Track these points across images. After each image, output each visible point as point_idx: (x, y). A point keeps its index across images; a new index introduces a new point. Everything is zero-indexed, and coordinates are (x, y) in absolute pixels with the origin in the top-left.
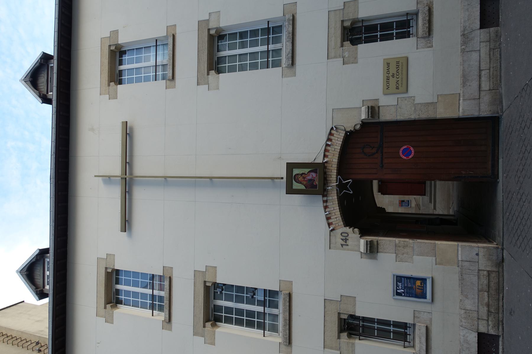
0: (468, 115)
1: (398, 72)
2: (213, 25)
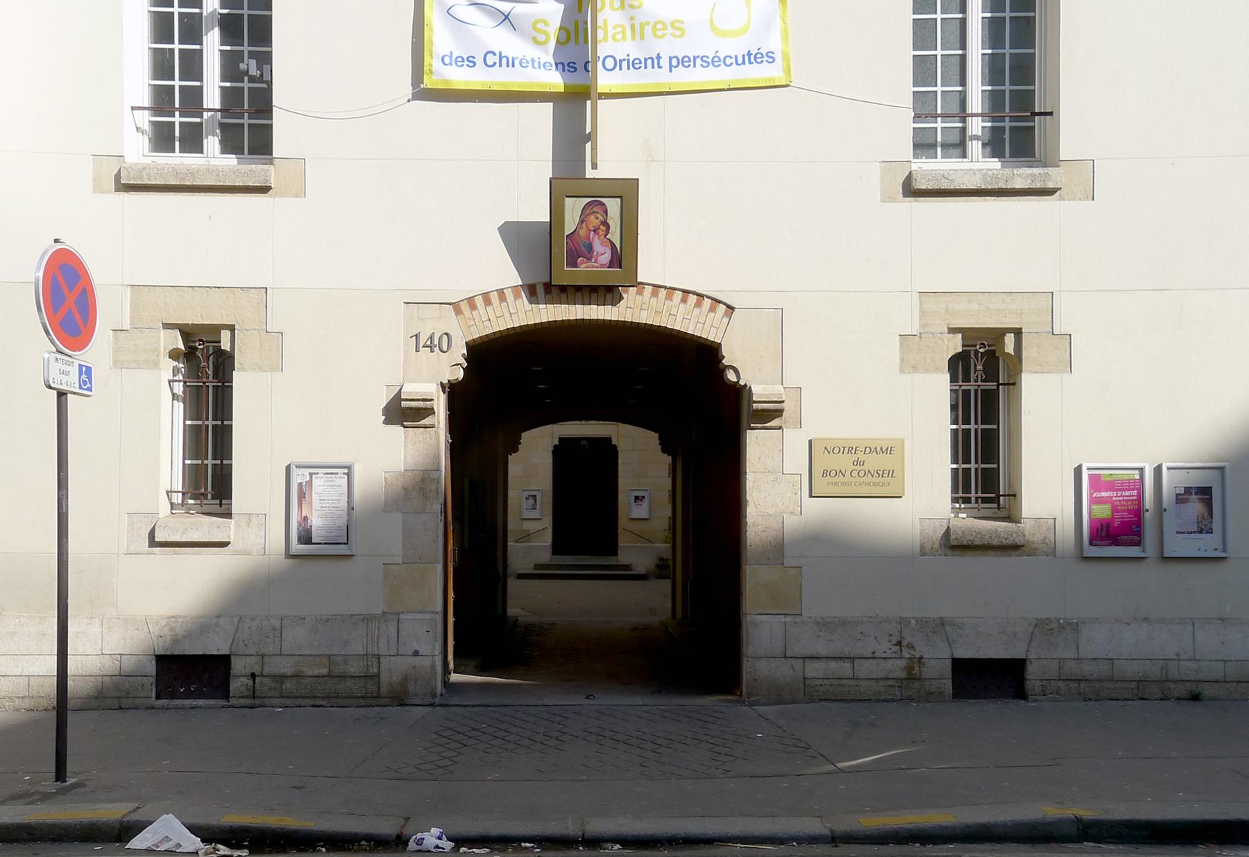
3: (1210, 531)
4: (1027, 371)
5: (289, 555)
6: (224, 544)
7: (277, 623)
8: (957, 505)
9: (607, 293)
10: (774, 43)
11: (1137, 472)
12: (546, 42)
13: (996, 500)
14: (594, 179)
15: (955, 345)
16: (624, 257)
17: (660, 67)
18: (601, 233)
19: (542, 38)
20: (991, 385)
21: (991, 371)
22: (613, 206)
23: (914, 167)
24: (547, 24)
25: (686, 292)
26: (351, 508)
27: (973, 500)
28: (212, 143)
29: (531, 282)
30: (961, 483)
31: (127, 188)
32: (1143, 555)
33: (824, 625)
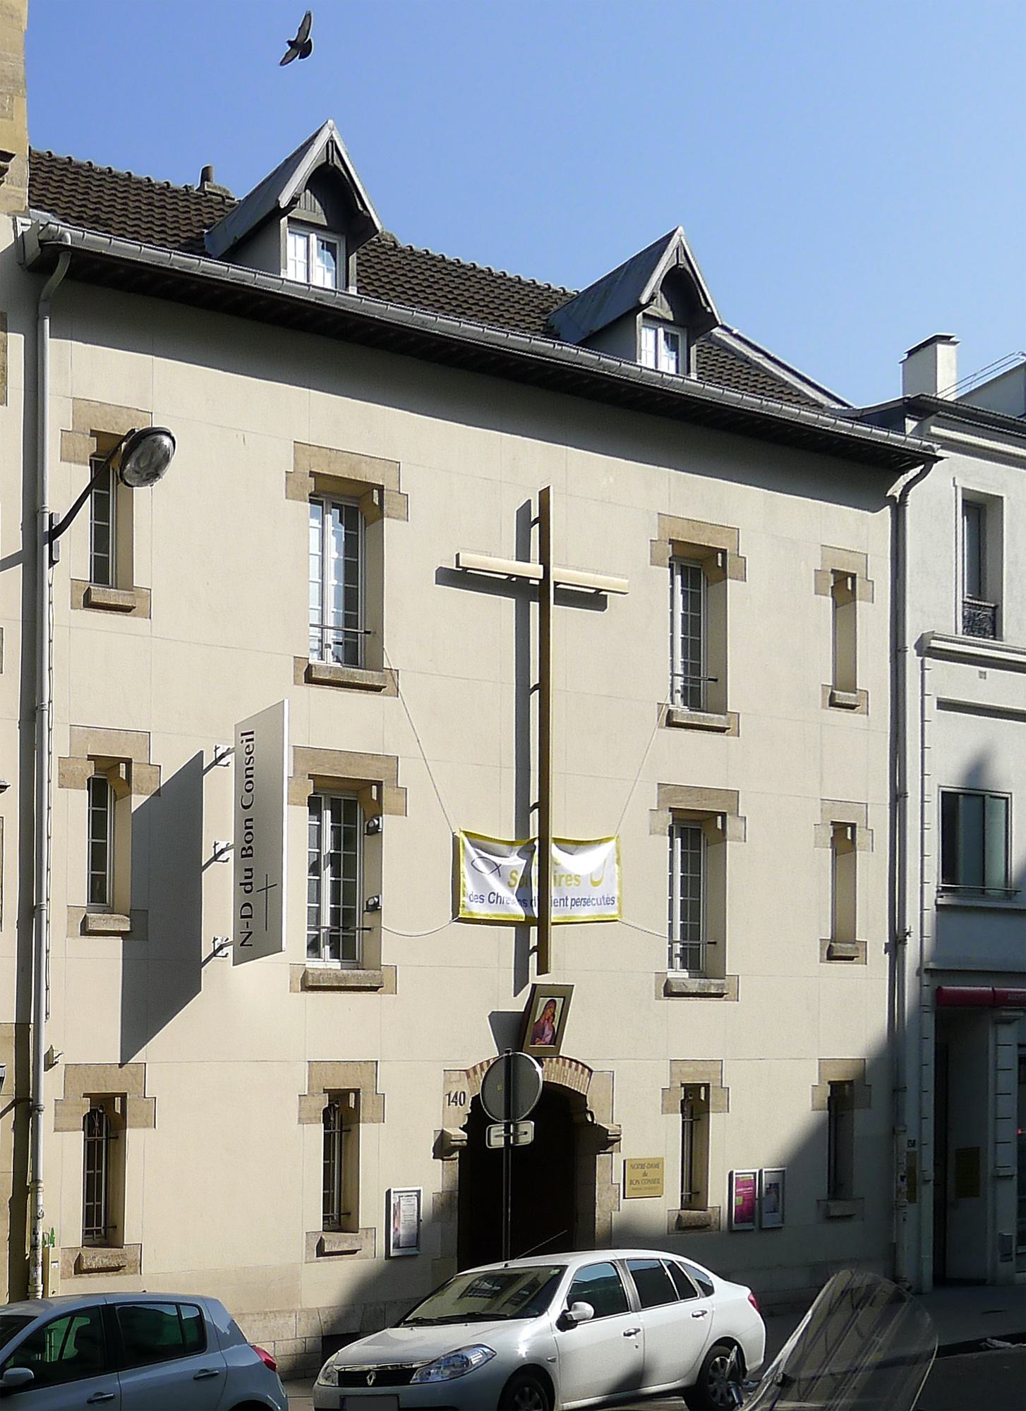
4: (131, 1127)
5: (388, 1256)
6: (354, 1252)
7: (382, 1307)
10: (616, 893)
11: (752, 1175)
12: (514, 886)
14: (553, 985)
16: (556, 1039)
19: (513, 882)
22: (559, 1001)
23: (669, 976)
25: (571, 1060)
26: (419, 1220)
28: (326, 950)
31: (307, 988)
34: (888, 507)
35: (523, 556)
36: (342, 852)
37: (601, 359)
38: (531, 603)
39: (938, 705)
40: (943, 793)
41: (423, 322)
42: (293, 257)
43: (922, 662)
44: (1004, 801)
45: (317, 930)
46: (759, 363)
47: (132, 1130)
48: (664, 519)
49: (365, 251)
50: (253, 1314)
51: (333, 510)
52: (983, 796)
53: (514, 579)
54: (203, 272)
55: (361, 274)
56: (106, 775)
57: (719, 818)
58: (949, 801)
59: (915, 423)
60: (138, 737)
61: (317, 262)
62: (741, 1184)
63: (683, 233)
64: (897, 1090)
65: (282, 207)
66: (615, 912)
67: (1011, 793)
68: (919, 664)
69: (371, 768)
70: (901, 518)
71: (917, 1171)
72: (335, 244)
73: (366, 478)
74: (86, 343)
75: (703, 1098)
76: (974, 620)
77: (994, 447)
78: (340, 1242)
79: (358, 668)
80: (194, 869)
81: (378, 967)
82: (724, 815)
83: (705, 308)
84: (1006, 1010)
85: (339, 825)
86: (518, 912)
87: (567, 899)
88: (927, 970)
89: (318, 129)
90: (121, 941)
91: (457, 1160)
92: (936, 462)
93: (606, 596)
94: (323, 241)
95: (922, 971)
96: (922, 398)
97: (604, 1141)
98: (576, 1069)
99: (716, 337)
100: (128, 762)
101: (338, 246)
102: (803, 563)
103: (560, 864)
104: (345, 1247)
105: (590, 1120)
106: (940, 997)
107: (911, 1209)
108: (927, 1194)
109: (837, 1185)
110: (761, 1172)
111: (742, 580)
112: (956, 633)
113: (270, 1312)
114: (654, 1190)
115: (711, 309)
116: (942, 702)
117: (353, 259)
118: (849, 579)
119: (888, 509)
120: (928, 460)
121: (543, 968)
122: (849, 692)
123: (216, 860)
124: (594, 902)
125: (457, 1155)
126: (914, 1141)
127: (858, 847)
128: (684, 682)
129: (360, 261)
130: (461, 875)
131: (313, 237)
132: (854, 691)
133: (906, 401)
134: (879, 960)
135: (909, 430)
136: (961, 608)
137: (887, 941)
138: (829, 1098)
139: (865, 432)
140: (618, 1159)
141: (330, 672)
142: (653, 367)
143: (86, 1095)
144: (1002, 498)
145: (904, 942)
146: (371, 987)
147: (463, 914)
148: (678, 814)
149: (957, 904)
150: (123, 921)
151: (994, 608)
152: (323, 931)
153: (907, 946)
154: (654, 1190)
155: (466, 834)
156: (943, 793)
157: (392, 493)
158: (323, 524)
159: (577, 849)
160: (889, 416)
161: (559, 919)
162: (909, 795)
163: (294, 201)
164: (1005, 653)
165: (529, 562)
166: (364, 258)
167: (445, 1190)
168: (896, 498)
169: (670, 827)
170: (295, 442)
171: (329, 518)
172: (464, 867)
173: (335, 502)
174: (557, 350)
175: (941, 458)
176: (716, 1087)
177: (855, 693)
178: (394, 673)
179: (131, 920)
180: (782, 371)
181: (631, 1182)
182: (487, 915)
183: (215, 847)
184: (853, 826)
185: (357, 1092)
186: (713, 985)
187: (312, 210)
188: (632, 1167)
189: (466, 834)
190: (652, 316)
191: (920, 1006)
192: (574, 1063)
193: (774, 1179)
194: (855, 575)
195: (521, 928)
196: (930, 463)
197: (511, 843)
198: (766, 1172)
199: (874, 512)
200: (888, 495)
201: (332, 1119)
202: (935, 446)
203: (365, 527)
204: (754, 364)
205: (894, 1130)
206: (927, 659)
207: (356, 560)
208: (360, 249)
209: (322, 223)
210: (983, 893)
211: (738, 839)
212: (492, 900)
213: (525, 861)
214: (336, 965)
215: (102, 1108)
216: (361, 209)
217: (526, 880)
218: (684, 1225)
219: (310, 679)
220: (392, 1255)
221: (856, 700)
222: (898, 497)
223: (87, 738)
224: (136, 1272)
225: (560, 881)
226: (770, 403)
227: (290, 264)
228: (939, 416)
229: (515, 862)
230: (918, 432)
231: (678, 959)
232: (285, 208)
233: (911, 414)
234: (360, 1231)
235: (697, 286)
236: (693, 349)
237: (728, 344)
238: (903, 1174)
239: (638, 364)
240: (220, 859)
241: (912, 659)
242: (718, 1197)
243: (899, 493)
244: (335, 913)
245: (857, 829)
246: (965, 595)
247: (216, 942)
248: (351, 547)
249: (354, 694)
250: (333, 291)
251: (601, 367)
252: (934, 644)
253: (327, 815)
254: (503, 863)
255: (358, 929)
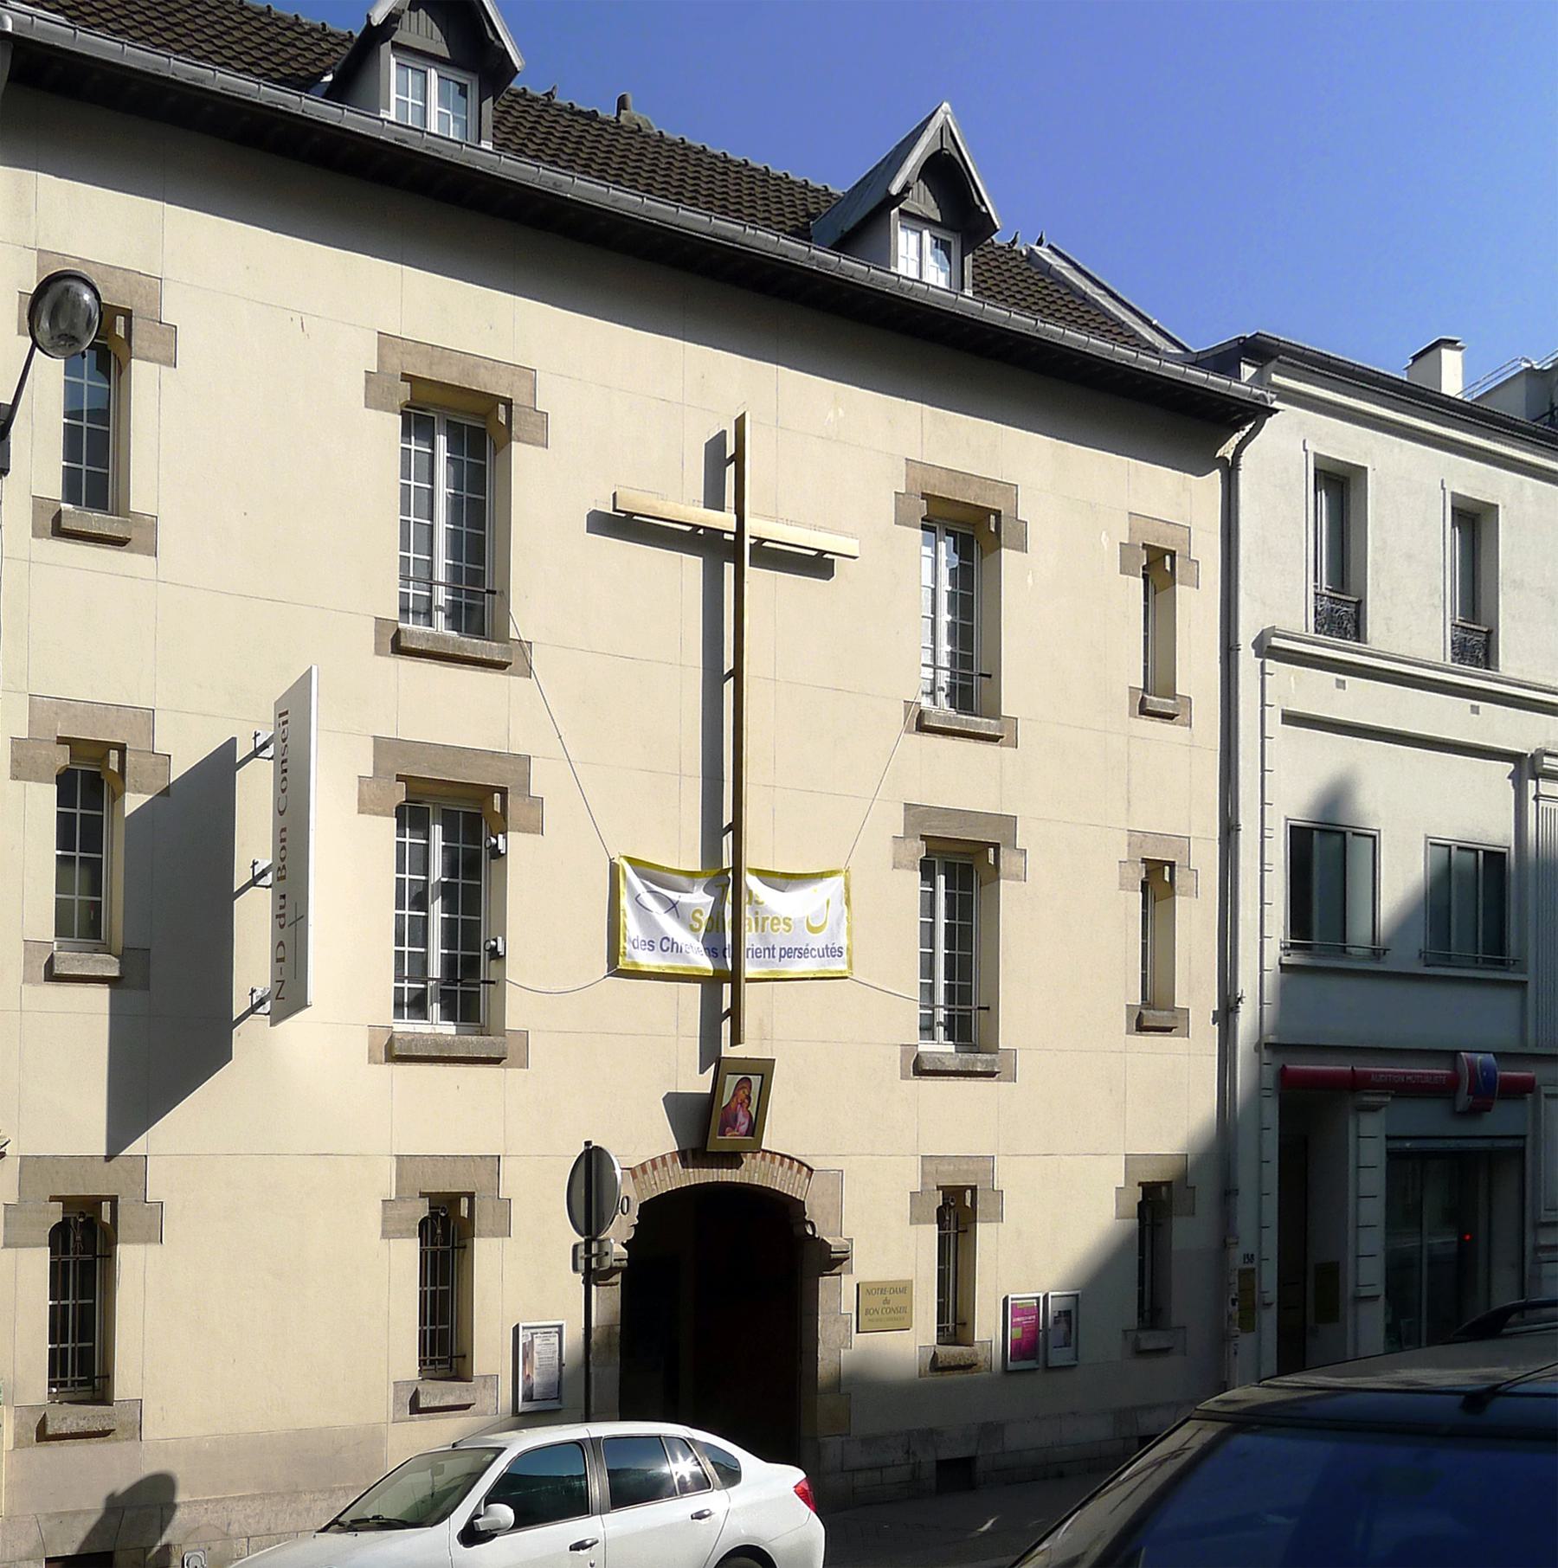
0: (1454, 1386)
1: (892, 1309)
2: (1007, 861)
3: (1070, 1346)
6: (466, 1407)
8: (54, 1390)
9: (732, 1159)
10: (843, 942)
12: (699, 930)
13: (90, 1382)
14: (746, 1059)
15: (56, 1214)
16: (755, 1128)
17: (774, 957)
18: (745, 1106)
19: (696, 925)
20: (89, 1257)
21: (89, 1245)
23: (921, 1048)
24: (701, 914)
25: (783, 1156)
26: (561, 1365)
27: (69, 1383)
28: (435, 1009)
29: (683, 1148)
30: (57, 1362)
32: (559, 1406)
33: (868, 1441)
34: (1217, 471)
35: (714, 500)
36: (460, 881)
37: (1163, 363)
38: (726, 564)
39: (1283, 719)
40: (1292, 827)
41: (555, 184)
42: (905, 255)
43: (1263, 664)
44: (1371, 840)
45: (930, 1009)
46: (1097, 301)
47: (983, 1225)
48: (914, 467)
49: (982, 253)
50: (312, 1492)
51: (947, 538)
52: (1344, 833)
53: (701, 532)
54: (222, 89)
55: (978, 278)
56: (99, 766)
57: (991, 850)
58: (1300, 838)
59: (1254, 370)
60: (135, 716)
61: (929, 259)
62: (1018, 1311)
63: (950, 110)
64: (1228, 1193)
65: (375, 24)
66: (844, 967)
67: (1379, 831)
68: (1259, 666)
69: (490, 769)
70: (1233, 487)
71: (1257, 1293)
72: (466, 85)
73: (485, 388)
74: (60, 177)
75: (968, 1204)
76: (1465, 646)
77: (1448, 434)
78: (443, 1395)
79: (972, 715)
80: (222, 897)
81: (502, 1032)
82: (997, 847)
83: (979, 207)
84: (1367, 1094)
85: (953, 891)
86: (705, 964)
87: (774, 949)
88: (1268, 1045)
89: (930, 113)
90: (108, 990)
91: (619, 1285)
92: (1271, 416)
93: (833, 560)
94: (935, 238)
95: (1267, 1047)
96: (1258, 337)
97: (832, 1261)
98: (790, 1167)
99: (1055, 269)
100: (122, 749)
101: (469, 87)
102: (1104, 533)
103: (762, 903)
104: (450, 1401)
105: (811, 1233)
106: (1286, 1081)
107: (1245, 1341)
108: (1268, 1320)
109: (1152, 1311)
110: (1046, 1298)
111: (543, 446)
112: (1307, 631)
113: (340, 1489)
114: (900, 1320)
115: (987, 209)
116: (1288, 716)
117: (969, 259)
118: (1168, 558)
119: (1217, 473)
120: (1257, 413)
121: (736, 1039)
122: (1165, 697)
123: (255, 885)
124: (814, 953)
125: (618, 1278)
126: (1252, 1255)
127: (1177, 891)
128: (951, 678)
129: (975, 263)
130: (622, 913)
131: (926, 233)
132: (1173, 696)
133: (1241, 341)
134: (1205, 1033)
135: (1245, 379)
136: (1313, 601)
137: (1216, 1009)
138: (1140, 1204)
139: (1177, 372)
140: (848, 1283)
141: (428, 640)
142: (917, 277)
143: (53, 1199)
144: (1365, 469)
145: (1235, 1010)
146: (488, 1058)
147: (624, 965)
148: (936, 845)
149: (1313, 964)
150: (108, 963)
151: (1489, 633)
152: (431, 983)
153: (1240, 1014)
154: (900, 1320)
155: (630, 860)
156: (1292, 827)
157: (523, 409)
158: (936, 554)
159: (788, 884)
160: (1225, 360)
161: (765, 973)
162: (1241, 827)
163: (906, 188)
164: (1366, 658)
165: (723, 511)
166: (982, 260)
167: (600, 1324)
168: (1228, 461)
169: (1142, 882)
170: (379, 333)
171: (942, 546)
172: (625, 902)
173: (450, 419)
174: (749, 235)
175: (1276, 411)
176: (985, 1190)
177: (1174, 699)
178: (524, 647)
179: (120, 962)
180: (1123, 309)
181: (867, 1312)
182: (659, 967)
183: (253, 867)
184: (1172, 865)
185: (471, 1196)
186: (980, 1062)
187: (923, 201)
188: (869, 1292)
189: (630, 860)
190: (912, 214)
191: (1260, 1090)
192: (787, 1160)
193: (1062, 1305)
194: (1175, 552)
195: (711, 984)
196: (1263, 416)
197: (691, 875)
198: (1052, 1297)
199: (1198, 476)
200: (1217, 456)
201: (947, 1218)
202: (1269, 395)
203: (982, 558)
204: (1092, 301)
205: (1225, 1241)
206: (1267, 660)
207: (483, 498)
208: (976, 251)
209: (443, 55)
210: (1345, 952)
211: (1016, 877)
212: (665, 948)
213: (713, 899)
214: (449, 1029)
215: (444, 1210)
216: (493, 38)
217: (716, 921)
218: (940, 1365)
219: (922, 727)
220: (520, 1410)
221: (1173, 707)
222: (1230, 458)
223: (56, 714)
224: (132, 1438)
225: (763, 926)
226: (1047, 325)
227: (901, 261)
228: (1279, 361)
229: (700, 899)
230: (1258, 380)
231: (942, 1028)
232: (378, 26)
233: (1246, 357)
234: (474, 1379)
235: (969, 180)
236: (969, 259)
237: (1067, 279)
238: (1234, 1297)
239: (893, 270)
240: (259, 883)
241: (1247, 660)
242: (988, 1327)
243: (1231, 454)
244: (449, 963)
245: (1176, 868)
246: (1458, 618)
247: (254, 995)
248: (964, 578)
249: (464, 671)
250: (459, 143)
251: (814, 262)
252: (1276, 642)
253: (941, 880)
254: (681, 900)
255: (484, 982)
